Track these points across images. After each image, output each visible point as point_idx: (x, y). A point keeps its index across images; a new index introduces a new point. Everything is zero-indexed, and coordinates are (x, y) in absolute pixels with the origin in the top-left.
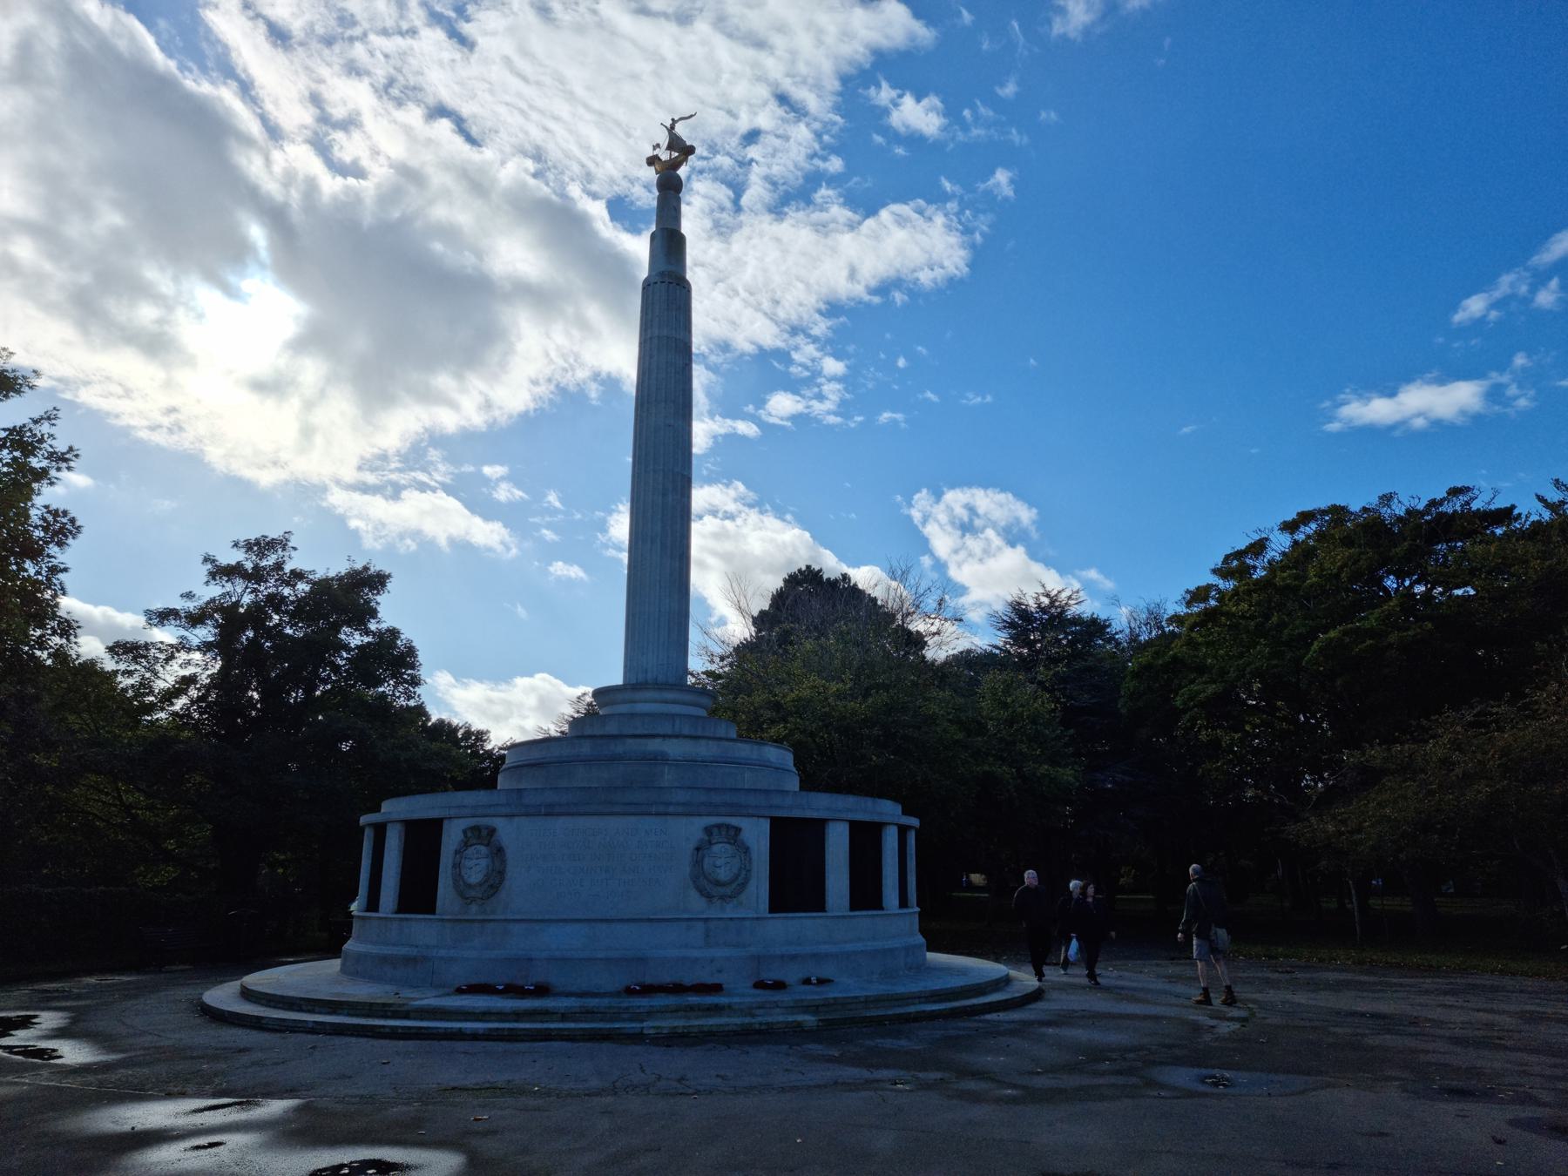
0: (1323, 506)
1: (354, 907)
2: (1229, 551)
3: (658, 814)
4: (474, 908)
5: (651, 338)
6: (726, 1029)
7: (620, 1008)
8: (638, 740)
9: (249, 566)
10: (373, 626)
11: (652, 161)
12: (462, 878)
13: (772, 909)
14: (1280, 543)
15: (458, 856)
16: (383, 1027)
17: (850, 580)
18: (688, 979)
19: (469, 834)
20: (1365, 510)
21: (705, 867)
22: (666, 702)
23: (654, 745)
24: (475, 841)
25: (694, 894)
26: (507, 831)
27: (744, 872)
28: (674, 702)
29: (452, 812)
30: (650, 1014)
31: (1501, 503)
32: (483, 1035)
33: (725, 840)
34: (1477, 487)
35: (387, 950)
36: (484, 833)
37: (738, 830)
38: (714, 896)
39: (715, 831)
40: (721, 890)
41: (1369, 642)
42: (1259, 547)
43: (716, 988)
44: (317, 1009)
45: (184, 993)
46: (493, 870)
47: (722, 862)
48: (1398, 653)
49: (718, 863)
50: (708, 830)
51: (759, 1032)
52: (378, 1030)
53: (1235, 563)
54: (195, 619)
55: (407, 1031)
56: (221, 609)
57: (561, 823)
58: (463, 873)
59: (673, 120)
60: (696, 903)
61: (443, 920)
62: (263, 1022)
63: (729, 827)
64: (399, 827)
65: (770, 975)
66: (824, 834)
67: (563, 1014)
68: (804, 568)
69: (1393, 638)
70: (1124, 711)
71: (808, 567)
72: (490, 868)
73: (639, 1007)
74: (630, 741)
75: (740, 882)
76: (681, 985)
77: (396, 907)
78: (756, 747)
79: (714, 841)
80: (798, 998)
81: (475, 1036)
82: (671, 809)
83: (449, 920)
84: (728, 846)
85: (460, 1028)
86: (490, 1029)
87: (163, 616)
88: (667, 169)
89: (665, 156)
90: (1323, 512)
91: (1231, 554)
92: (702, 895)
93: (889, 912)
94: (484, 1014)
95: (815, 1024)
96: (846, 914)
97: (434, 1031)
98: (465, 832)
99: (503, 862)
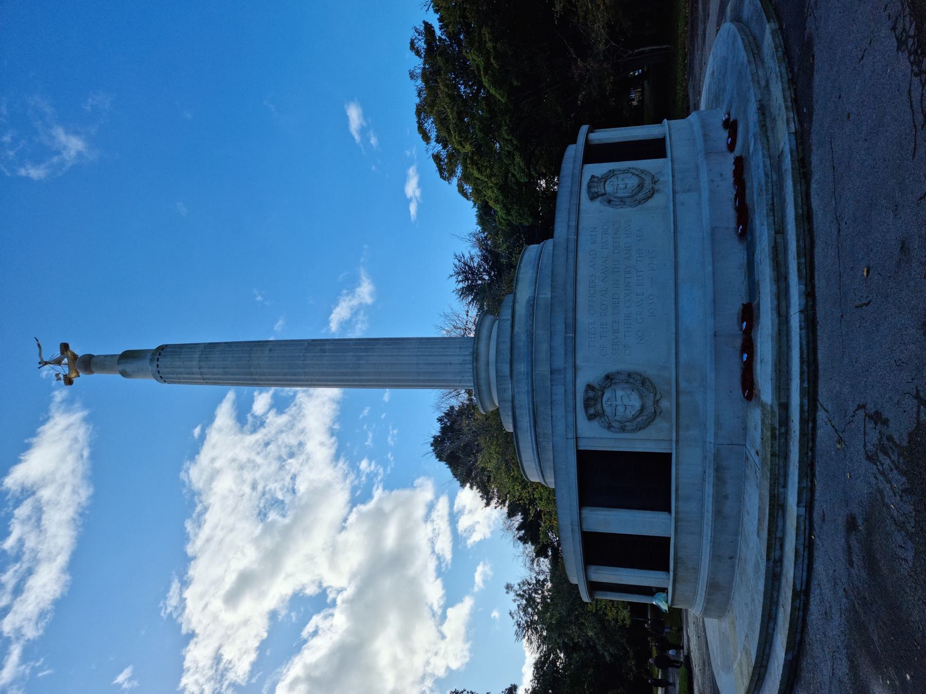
0: (416, 119)
1: (664, 607)
2: (438, 174)
3: (577, 234)
4: (665, 404)
5: (200, 368)
8: (516, 323)
12: (635, 418)
15: (613, 424)
20: (419, 95)
22: (489, 337)
25: (651, 203)
26: (589, 374)
28: (490, 332)
33: (602, 184)
35: (709, 516)
36: (591, 394)
37: (593, 177)
41: (492, 60)
42: (437, 158)
44: (779, 534)
46: (627, 382)
48: (499, 43)
49: (622, 186)
55: (805, 377)
57: (583, 318)
60: (658, 200)
61: (677, 441)
67: (777, 233)
68: (433, 448)
69: (489, 45)
71: (432, 445)
72: (626, 386)
74: (516, 329)
77: (665, 572)
79: (603, 191)
82: (573, 224)
83: (677, 432)
86: (800, 277)
97: (804, 342)
98: (591, 418)
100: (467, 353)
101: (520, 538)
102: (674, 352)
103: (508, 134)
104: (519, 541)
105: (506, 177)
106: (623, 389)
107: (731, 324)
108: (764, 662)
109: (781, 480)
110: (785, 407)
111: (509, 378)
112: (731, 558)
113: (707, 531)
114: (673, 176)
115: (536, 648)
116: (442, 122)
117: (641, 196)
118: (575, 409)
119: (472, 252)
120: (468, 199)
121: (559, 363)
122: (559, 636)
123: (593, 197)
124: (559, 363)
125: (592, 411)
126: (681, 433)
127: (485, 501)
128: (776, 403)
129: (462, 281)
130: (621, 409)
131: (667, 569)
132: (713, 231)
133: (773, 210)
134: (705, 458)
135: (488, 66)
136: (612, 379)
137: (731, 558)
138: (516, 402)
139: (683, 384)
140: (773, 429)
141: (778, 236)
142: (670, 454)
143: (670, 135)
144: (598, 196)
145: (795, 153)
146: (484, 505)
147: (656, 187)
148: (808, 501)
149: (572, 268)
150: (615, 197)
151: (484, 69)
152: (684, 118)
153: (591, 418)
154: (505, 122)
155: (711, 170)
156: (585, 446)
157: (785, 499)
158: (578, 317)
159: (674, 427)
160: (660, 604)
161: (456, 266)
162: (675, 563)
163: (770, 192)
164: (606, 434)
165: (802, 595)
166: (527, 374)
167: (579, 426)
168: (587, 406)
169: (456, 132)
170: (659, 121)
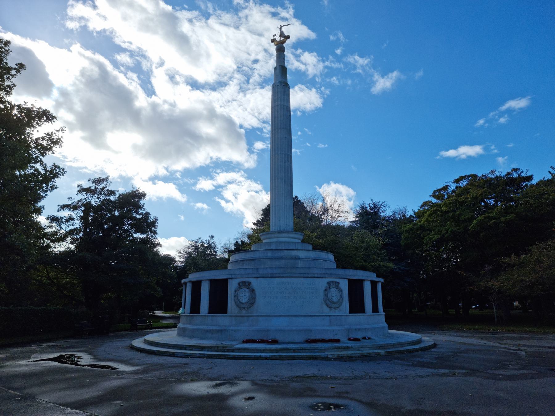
0: (468, 174)
2: (435, 189)
3: (311, 277)
4: (244, 311)
5: (277, 105)
6: (356, 355)
7: (314, 348)
8: (288, 251)
9: (93, 188)
10: (140, 211)
11: (273, 41)
12: (239, 300)
13: (350, 312)
14: (453, 186)
15: (236, 292)
16: (229, 355)
17: (298, 198)
18: (327, 337)
19: (241, 284)
20: (483, 176)
21: (329, 297)
23: (294, 253)
24: (243, 287)
25: (325, 306)
26: (255, 283)
27: (341, 299)
28: (292, 238)
29: (233, 276)
30: (325, 350)
31: (529, 174)
32: (269, 358)
33: (335, 287)
34: (521, 168)
36: (247, 284)
37: (339, 283)
38: (332, 307)
39: (332, 284)
40: (335, 305)
41: (493, 221)
42: (445, 188)
43: (338, 341)
44: (194, 349)
45: (125, 342)
47: (334, 295)
49: (333, 295)
50: (329, 283)
51: (366, 356)
52: (227, 356)
53: (437, 194)
54: (74, 208)
55: (238, 356)
56: (83, 205)
57: (276, 281)
58: (239, 299)
59: (281, 26)
60: (326, 310)
61: (231, 316)
62: (175, 354)
63: (336, 282)
64: (208, 282)
65: (352, 336)
66: (363, 285)
69: (502, 219)
70: (403, 244)
72: (250, 297)
73: (321, 347)
74: (286, 251)
75: (340, 302)
76: (324, 339)
78: (327, 254)
80: (373, 344)
81: (266, 358)
82: (316, 276)
84: (335, 289)
85: (260, 355)
86: (272, 356)
87: (64, 207)
88: (280, 44)
89: (278, 38)
90: (468, 176)
91: (436, 190)
92: (328, 307)
93: (367, 314)
94: (264, 350)
95: (384, 353)
96: (347, 314)
97: (250, 356)
98: (239, 284)
99: (255, 294)
100: (284, 227)
101: (237, 242)
102: (262, 315)
103: (451, 231)
104: (235, 242)
105: (428, 230)
106: (249, 296)
107: (271, 337)
108: (156, 345)
109: (210, 350)
110: (233, 351)
111: (265, 249)
112: (193, 336)
113: (201, 327)
114: (338, 316)
115: (186, 251)
116: (466, 190)
117: (328, 302)
118: (242, 278)
119: (387, 212)
120: (421, 207)
121: (261, 271)
122: (190, 264)
123: (329, 283)
124: (261, 271)
125: (241, 284)
126: (234, 318)
127: (256, 222)
128: (234, 348)
129: (370, 207)
130: (241, 295)
131: (191, 313)
132: (310, 331)
133: (302, 349)
134: (225, 326)
135: (490, 219)
136: (252, 292)
137: (193, 336)
138: (256, 252)
139: (251, 318)
140: (226, 347)
141: (292, 351)
142: (227, 314)
143: (379, 315)
144: (329, 285)
145: (319, 356)
146: (254, 222)
147: (332, 309)
148: (200, 356)
149: (296, 275)
150: (328, 292)
151: (489, 216)
152: (385, 322)
153: (239, 284)
154: (459, 229)
155: (339, 330)
156: (230, 281)
157: (204, 351)
158: (277, 278)
159: (236, 315)
160: (181, 310)
161: (378, 203)
162: (192, 316)
163: (310, 349)
164: (233, 290)
165: (173, 355)
166: (267, 257)
167: (235, 280)
168: (242, 282)
169: (452, 201)
170: (384, 311)
